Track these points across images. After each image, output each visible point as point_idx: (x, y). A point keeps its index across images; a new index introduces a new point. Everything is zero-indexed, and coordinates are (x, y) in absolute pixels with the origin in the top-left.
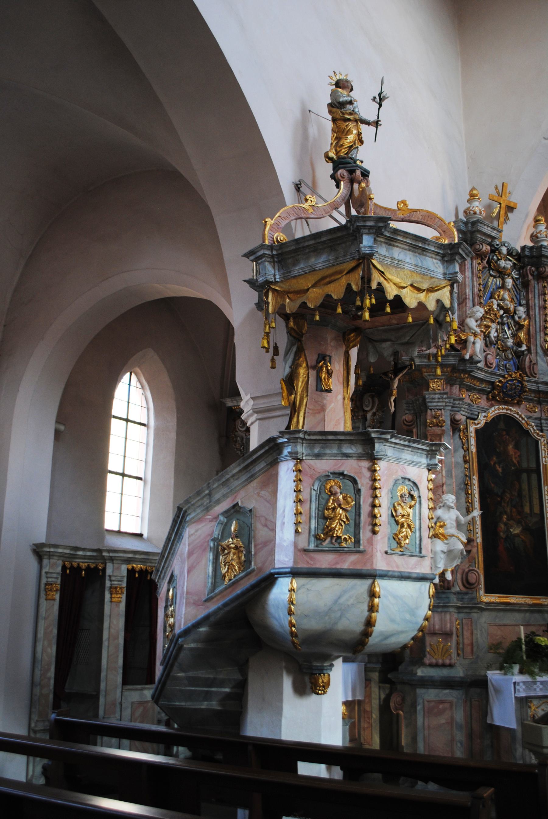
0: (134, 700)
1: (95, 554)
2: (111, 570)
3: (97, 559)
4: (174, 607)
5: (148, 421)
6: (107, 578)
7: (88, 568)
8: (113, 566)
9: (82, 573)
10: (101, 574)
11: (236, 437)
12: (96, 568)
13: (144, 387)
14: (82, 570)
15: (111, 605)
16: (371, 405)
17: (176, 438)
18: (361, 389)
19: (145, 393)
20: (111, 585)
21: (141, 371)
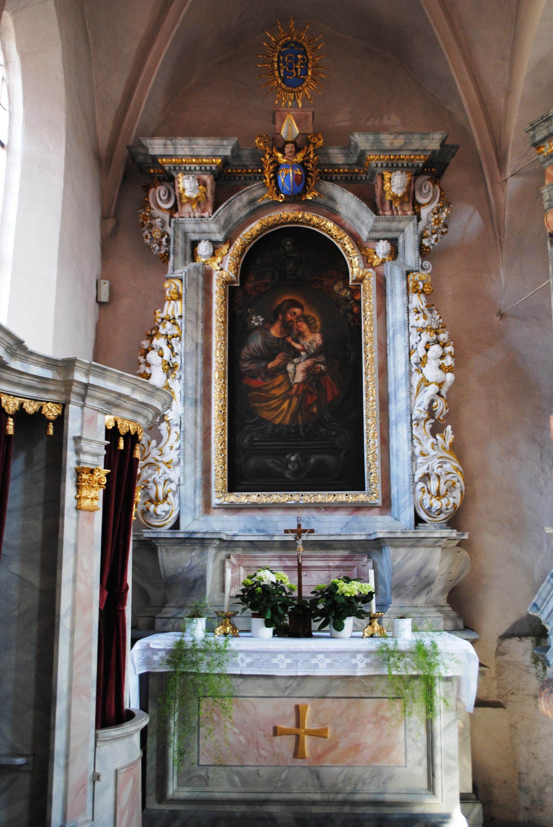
0: (119, 765)
1: (48, 374)
2: (78, 424)
3: (46, 391)
4: (469, 536)
5: (9, 139)
6: (70, 444)
7: (21, 411)
8: (83, 414)
9: (6, 423)
10: (51, 432)
11: (153, 218)
12: (39, 415)
13: (10, 64)
14: (8, 415)
15: (78, 519)
16: (431, 195)
17: (62, 186)
18: (421, 165)
19: (8, 77)
20: (79, 463)
21: (15, 25)
